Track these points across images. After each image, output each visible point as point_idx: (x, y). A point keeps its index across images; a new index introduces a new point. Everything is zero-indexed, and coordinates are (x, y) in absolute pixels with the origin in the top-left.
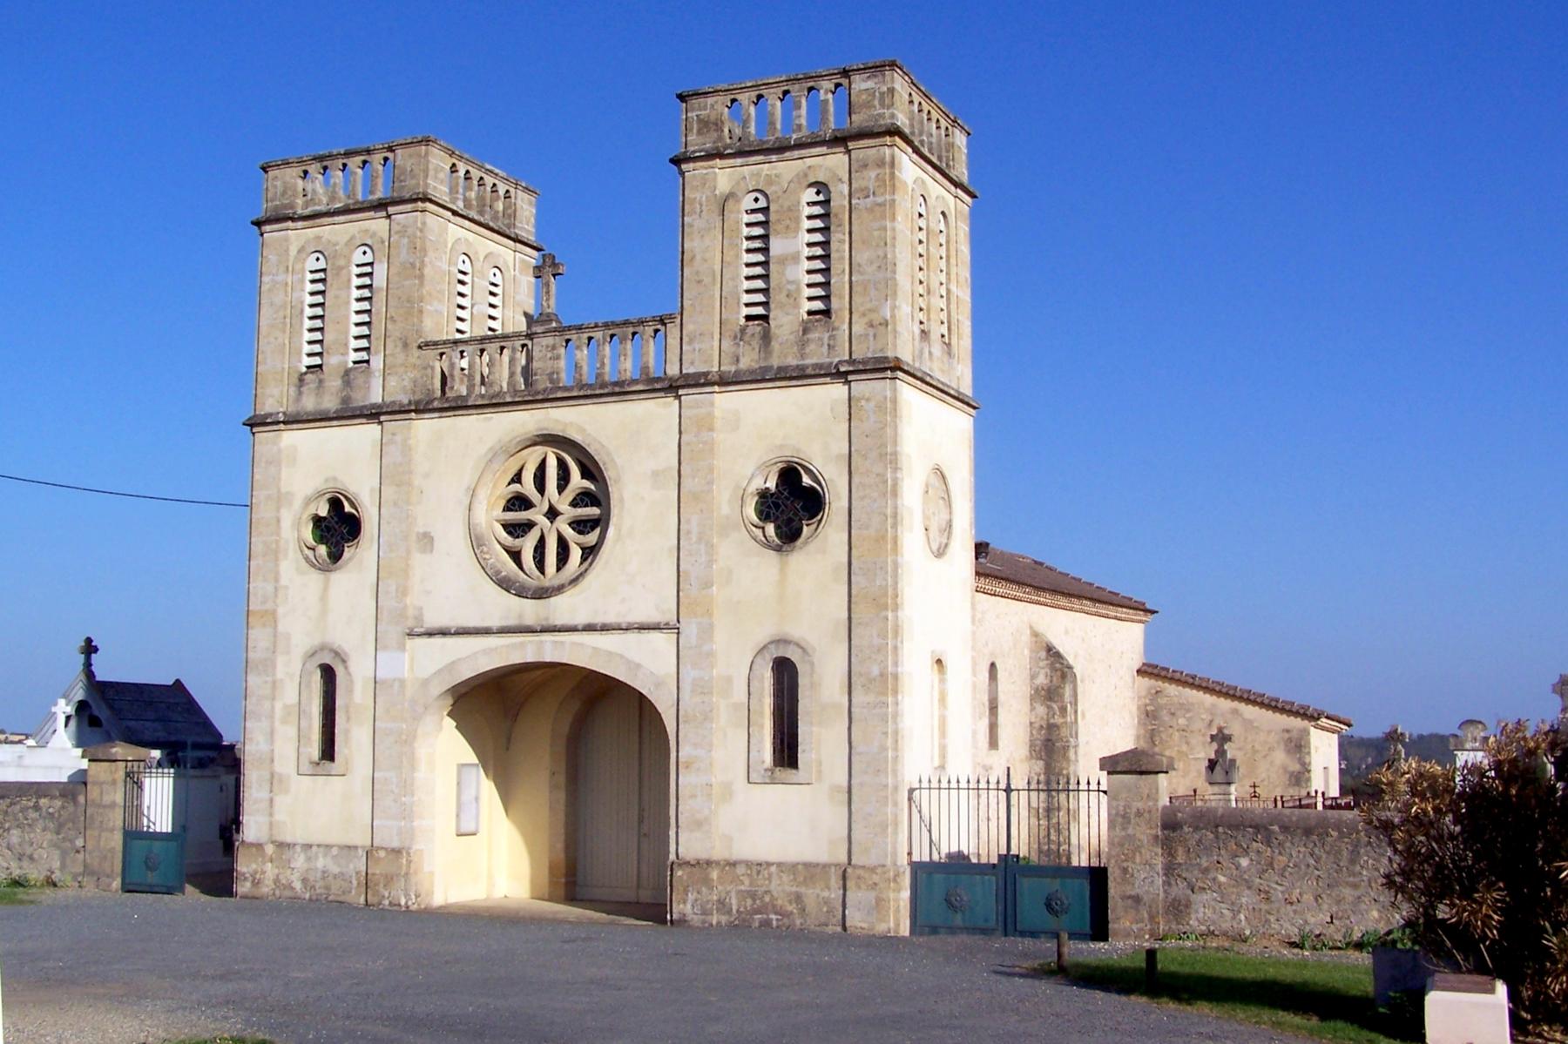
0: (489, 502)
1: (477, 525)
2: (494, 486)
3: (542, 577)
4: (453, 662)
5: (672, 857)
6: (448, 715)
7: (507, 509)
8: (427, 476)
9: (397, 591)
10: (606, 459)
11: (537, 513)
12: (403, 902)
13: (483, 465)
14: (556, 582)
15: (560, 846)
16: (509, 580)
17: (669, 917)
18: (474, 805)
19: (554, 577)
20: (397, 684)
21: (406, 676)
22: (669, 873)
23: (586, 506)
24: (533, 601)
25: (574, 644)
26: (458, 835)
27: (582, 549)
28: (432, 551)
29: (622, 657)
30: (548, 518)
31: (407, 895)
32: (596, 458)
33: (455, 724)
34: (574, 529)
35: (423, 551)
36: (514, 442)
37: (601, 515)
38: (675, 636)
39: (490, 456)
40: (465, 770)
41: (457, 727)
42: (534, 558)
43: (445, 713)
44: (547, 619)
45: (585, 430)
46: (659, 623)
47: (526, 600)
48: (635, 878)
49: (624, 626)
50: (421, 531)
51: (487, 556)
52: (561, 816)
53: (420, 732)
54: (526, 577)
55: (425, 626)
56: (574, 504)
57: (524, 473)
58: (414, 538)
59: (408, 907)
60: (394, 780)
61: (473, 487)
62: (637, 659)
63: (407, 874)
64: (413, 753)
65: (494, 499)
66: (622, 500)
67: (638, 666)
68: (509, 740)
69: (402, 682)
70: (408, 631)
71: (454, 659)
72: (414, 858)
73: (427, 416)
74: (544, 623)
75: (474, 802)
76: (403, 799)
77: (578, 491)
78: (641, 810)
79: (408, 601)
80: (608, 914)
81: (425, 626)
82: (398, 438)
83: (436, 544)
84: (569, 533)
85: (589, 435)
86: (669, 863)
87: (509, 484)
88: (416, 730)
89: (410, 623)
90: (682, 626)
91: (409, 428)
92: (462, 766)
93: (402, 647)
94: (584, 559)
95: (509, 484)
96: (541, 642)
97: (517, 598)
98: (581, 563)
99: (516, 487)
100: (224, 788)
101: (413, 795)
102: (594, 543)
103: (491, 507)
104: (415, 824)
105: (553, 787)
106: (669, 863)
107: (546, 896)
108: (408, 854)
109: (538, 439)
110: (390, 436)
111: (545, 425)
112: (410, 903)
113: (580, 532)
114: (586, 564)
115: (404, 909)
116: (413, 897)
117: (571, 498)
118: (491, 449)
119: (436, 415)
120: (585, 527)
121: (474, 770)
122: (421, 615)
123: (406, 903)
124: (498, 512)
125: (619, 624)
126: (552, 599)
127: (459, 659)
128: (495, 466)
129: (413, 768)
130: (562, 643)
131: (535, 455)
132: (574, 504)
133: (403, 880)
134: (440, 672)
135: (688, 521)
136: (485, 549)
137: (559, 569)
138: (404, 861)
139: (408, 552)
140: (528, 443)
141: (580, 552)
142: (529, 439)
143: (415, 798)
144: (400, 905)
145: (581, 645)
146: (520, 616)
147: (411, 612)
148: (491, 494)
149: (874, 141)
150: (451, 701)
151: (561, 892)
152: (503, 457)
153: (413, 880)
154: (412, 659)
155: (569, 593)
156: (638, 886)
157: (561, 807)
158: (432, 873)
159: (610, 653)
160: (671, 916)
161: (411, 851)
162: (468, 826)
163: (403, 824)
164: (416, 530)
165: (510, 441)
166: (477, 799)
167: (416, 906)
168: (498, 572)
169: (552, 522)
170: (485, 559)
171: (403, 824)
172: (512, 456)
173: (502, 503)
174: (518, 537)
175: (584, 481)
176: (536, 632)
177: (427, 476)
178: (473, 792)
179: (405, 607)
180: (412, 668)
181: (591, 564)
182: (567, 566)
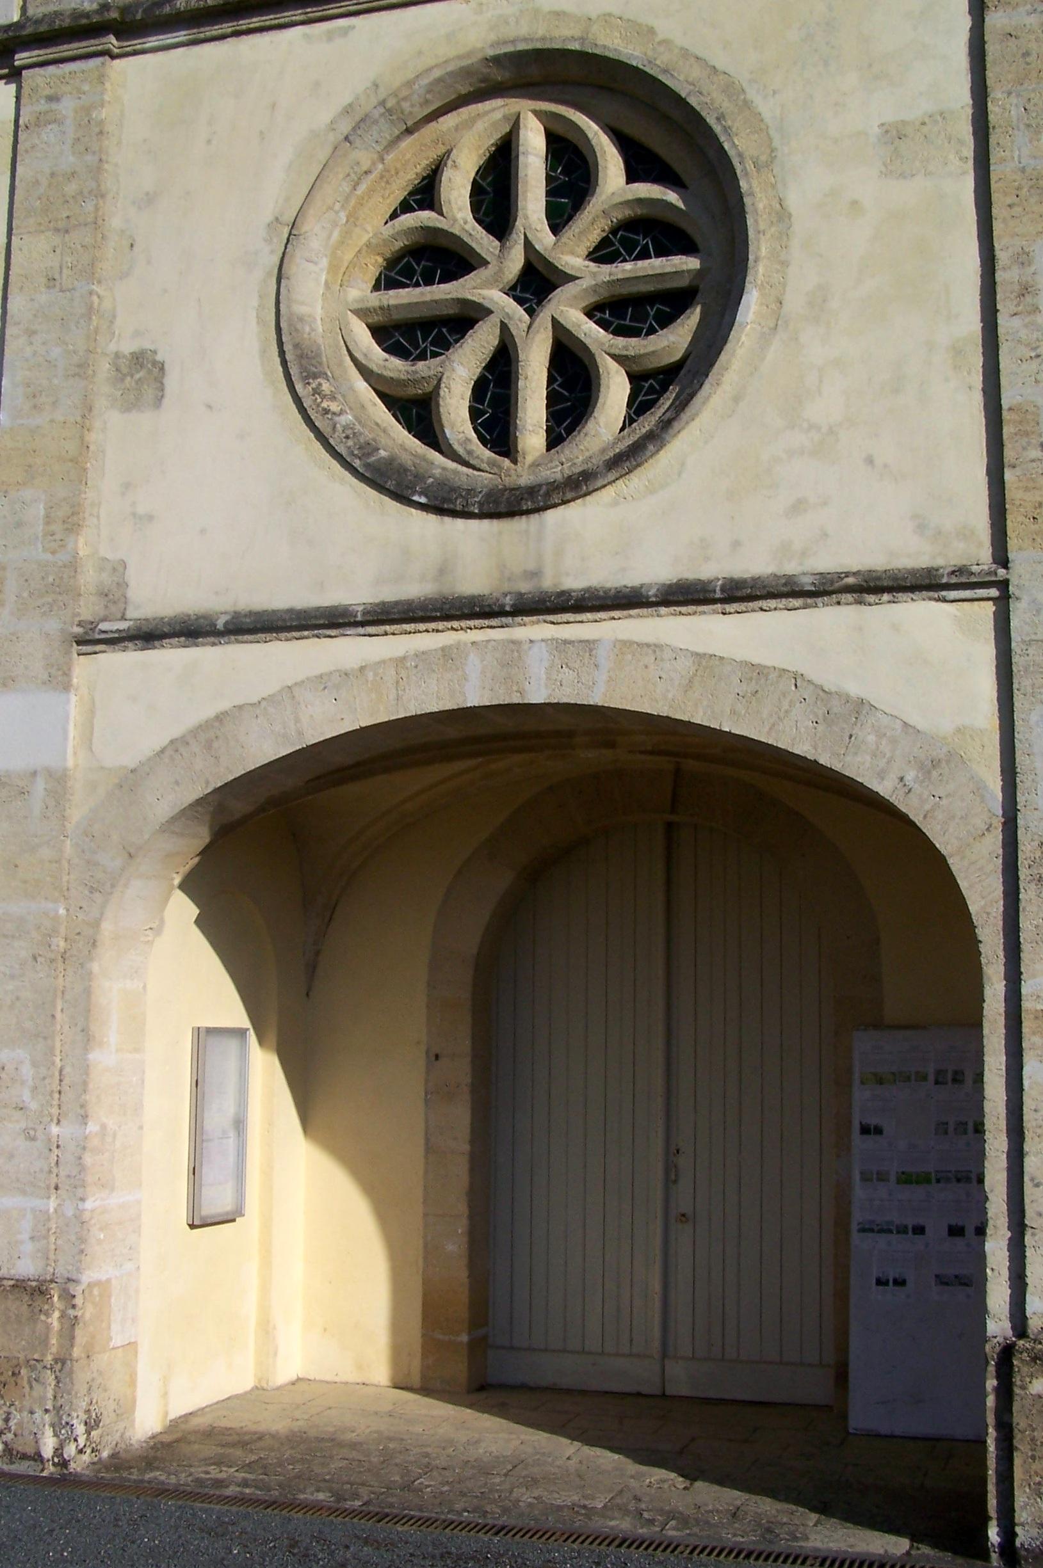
0: (333, 268)
1: (301, 319)
2: (352, 217)
3: (506, 462)
4: (220, 718)
5: (998, 1326)
6: (182, 887)
7: (386, 281)
8: (149, 200)
9: (48, 519)
10: (726, 105)
11: (487, 284)
12: (48, 1451)
13: (323, 155)
14: (557, 469)
15: (455, 1247)
16: (403, 470)
17: (993, 1534)
18: (231, 1142)
19: (535, 465)
20: (40, 785)
21: (70, 763)
22: (991, 1383)
23: (644, 255)
24: (486, 523)
25: (626, 646)
26: (192, 1226)
27: (633, 378)
28: (159, 400)
29: (797, 679)
30: (520, 301)
31: (61, 1426)
32: (693, 101)
33: (195, 911)
34: (601, 323)
35: (131, 404)
36: (425, 81)
37: (699, 273)
38: (990, 607)
39: (345, 127)
40: (213, 1042)
41: (198, 922)
42: (474, 414)
43: (177, 881)
44: (535, 574)
45: (651, 31)
46: (930, 572)
47: (460, 523)
48: (657, 1332)
49: (807, 583)
50: (128, 347)
51: (334, 407)
52: (459, 1171)
53: (107, 927)
54: (451, 465)
55: (132, 613)
56: (602, 253)
57: (447, 174)
58: (104, 367)
59: (64, 1464)
60: (27, 1071)
61: (289, 217)
62: (854, 689)
63: (62, 1361)
64: (88, 992)
65: (349, 256)
66: (782, 215)
67: (860, 707)
68: (312, 969)
69: (59, 780)
70: (78, 630)
71: (224, 705)
72: (86, 1311)
73: (153, 41)
74: (525, 587)
75: (232, 1134)
76: (55, 1130)
77: (619, 215)
78: (672, 1153)
79: (82, 545)
80: (691, 1475)
81: (132, 613)
82: (67, 107)
83: (172, 382)
84: (590, 332)
85: (665, 42)
86: (991, 1350)
87: (394, 216)
88: (96, 924)
89: (88, 608)
90: (1020, 573)
91: (101, 79)
92: (205, 1036)
93: (60, 680)
94: (638, 407)
95: (394, 216)
96: (516, 643)
97: (432, 518)
98: (629, 421)
99: (425, 217)
100: (683, 1219)
101: (84, 1118)
102: (677, 356)
103: (340, 275)
104: (89, 1205)
105: (435, 1094)
106: (991, 1350)
107: (416, 1381)
108: (69, 1298)
109: (499, 75)
110: (43, 106)
111: (511, 32)
112: (70, 1450)
113: (621, 332)
114: (647, 423)
115: (50, 1469)
116: (80, 1429)
117: (594, 237)
118: (348, 110)
119: (182, 36)
120: (641, 317)
121: (233, 1044)
122: (123, 585)
123: (58, 1451)
124: (360, 291)
125: (790, 580)
126: (551, 515)
127: (240, 708)
128: (363, 156)
129: (87, 1038)
130: (589, 645)
131: (480, 126)
132: (602, 253)
133: (50, 1378)
134: (176, 745)
135: (1023, 258)
136: (326, 387)
137: (554, 440)
138: (54, 1320)
139: (88, 409)
140: (464, 89)
141: (627, 387)
142: (466, 72)
143: (92, 1127)
144: (38, 1457)
145: (656, 648)
146: (442, 571)
147: (89, 578)
148: (342, 243)
149: (253, 636)
150: (202, 836)
151: (459, 1369)
152: (387, 131)
153: (82, 1376)
154: (91, 713)
155: (608, 494)
156: (664, 1355)
157: (459, 1141)
158: (131, 1347)
159: (758, 671)
160: (1008, 1533)
161: (77, 1290)
162: (217, 1200)
163: (52, 1204)
164: (112, 347)
165: (409, 84)
166: (240, 1124)
167: (86, 1458)
168: (368, 449)
169: (531, 312)
170: (326, 411)
171: (52, 1204)
172: (409, 131)
173: (374, 266)
174: (422, 357)
175: (636, 186)
176: (502, 613)
177: (149, 200)
178: (231, 1110)
179: (73, 565)
180: (87, 739)
181: (666, 424)
182: (591, 426)
